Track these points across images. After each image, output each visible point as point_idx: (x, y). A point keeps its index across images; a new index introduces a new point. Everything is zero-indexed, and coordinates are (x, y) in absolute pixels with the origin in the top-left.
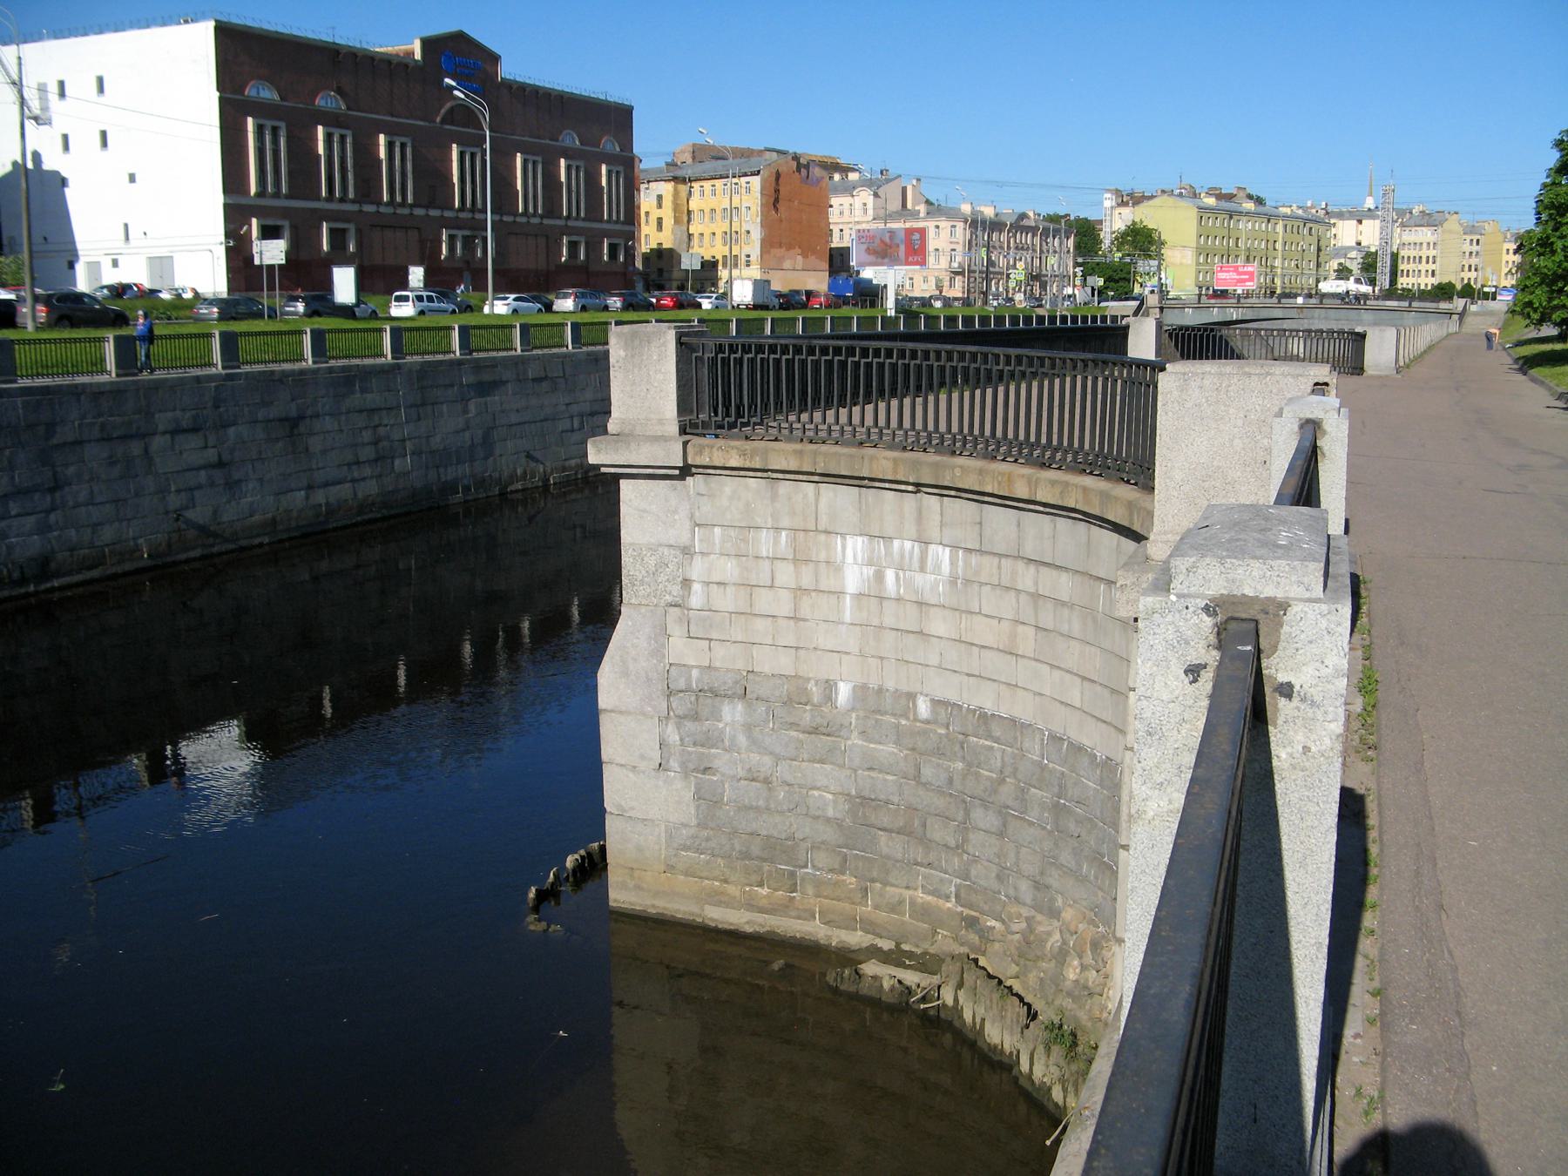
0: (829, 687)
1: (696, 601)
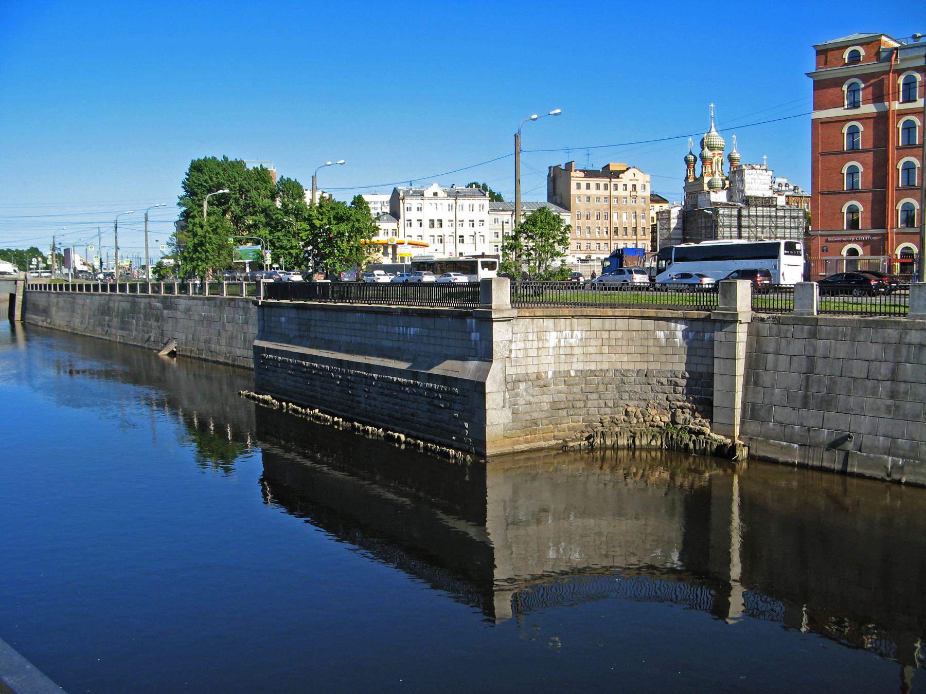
0: (546, 373)
1: (513, 355)
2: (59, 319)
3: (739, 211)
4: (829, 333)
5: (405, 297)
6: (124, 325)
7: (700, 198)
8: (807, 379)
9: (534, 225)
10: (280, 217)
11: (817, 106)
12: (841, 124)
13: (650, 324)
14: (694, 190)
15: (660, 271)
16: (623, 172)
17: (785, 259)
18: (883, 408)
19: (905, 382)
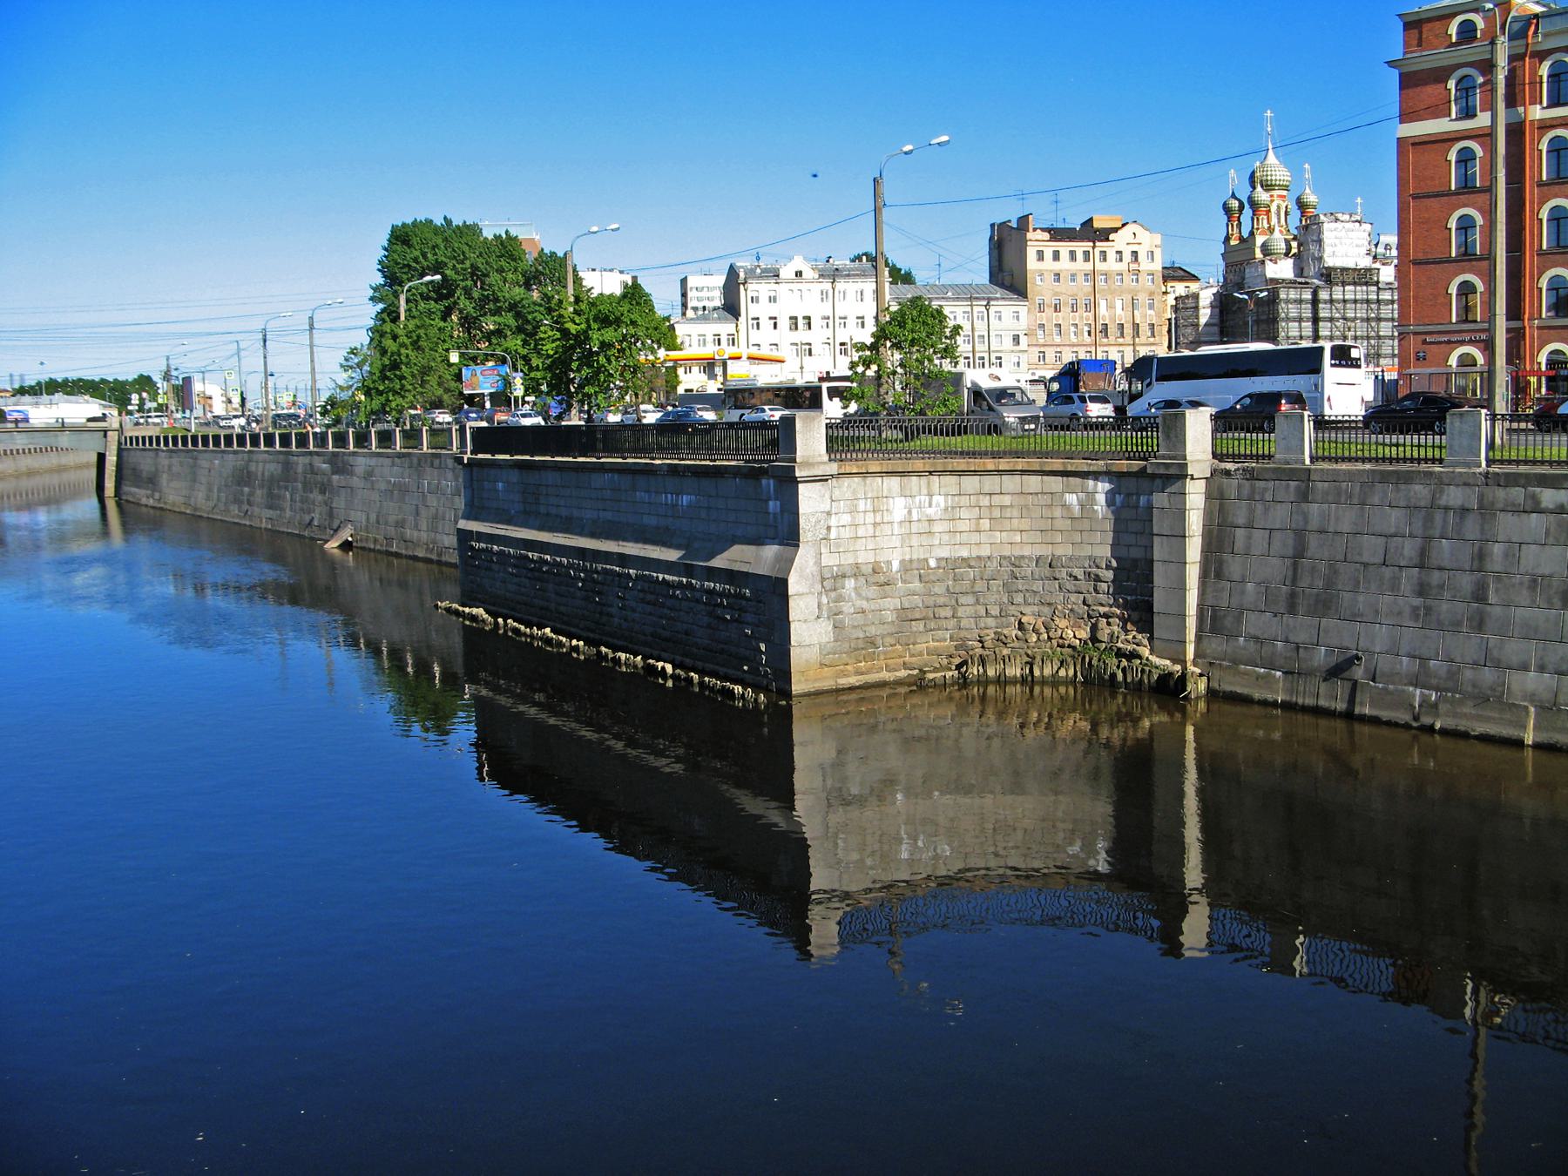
0: (889, 563)
1: (833, 535)
2: (173, 493)
3: (1315, 294)
4: (1327, 493)
5: (675, 449)
6: (273, 502)
7: (1249, 272)
8: (1295, 566)
9: (902, 325)
10: (539, 317)
11: (1406, 116)
12: (1446, 145)
13: (1056, 483)
14: (1239, 259)
15: (1134, 397)
16: (1116, 230)
17: (1332, 374)
18: (1407, 610)
19: (1440, 569)
